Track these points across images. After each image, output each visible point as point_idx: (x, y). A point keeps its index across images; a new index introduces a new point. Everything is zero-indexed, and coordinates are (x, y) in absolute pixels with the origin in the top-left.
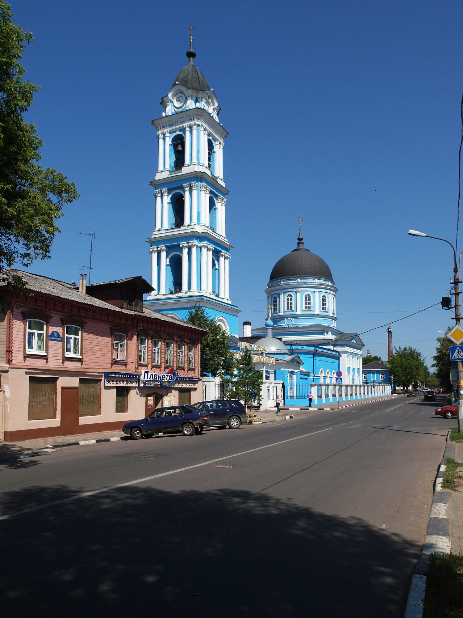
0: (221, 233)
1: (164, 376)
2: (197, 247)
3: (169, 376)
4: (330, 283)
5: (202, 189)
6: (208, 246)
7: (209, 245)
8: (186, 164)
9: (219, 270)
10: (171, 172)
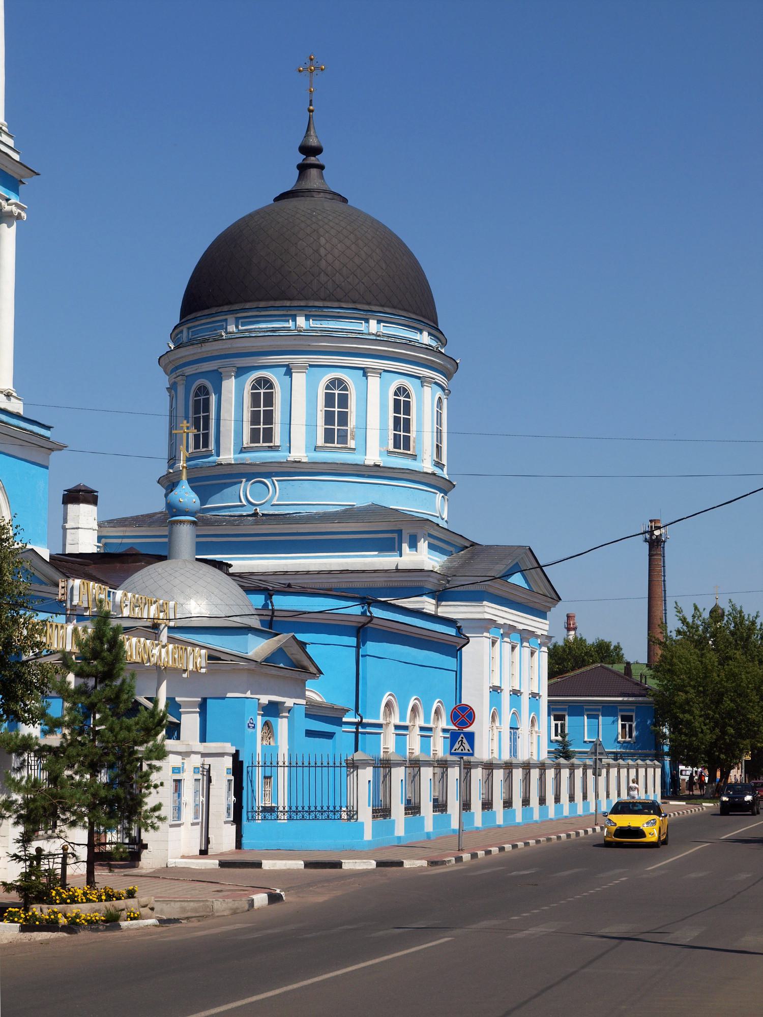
4: (425, 338)
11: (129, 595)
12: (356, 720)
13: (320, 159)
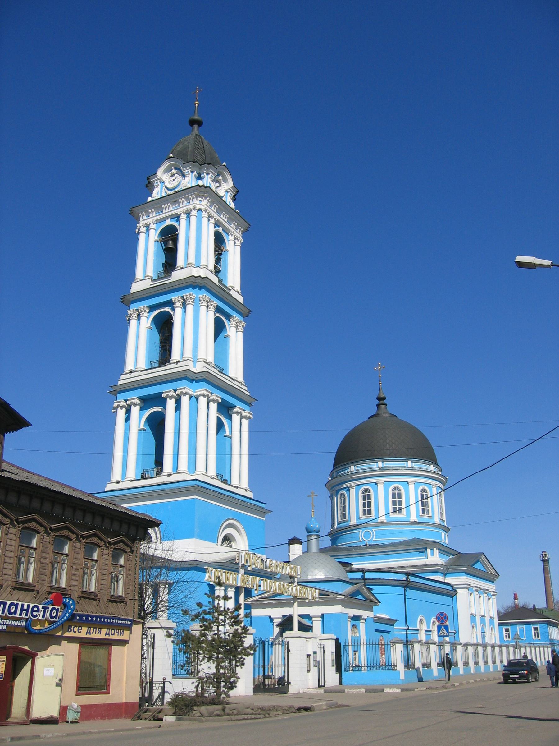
0: (235, 376)
1: (36, 609)
2: (191, 397)
3: (50, 610)
4: (432, 468)
5: (202, 303)
6: (210, 395)
7: (212, 394)
8: (178, 267)
9: (231, 438)
10: (154, 280)
11: (274, 562)
12: (406, 628)
13: (385, 402)
